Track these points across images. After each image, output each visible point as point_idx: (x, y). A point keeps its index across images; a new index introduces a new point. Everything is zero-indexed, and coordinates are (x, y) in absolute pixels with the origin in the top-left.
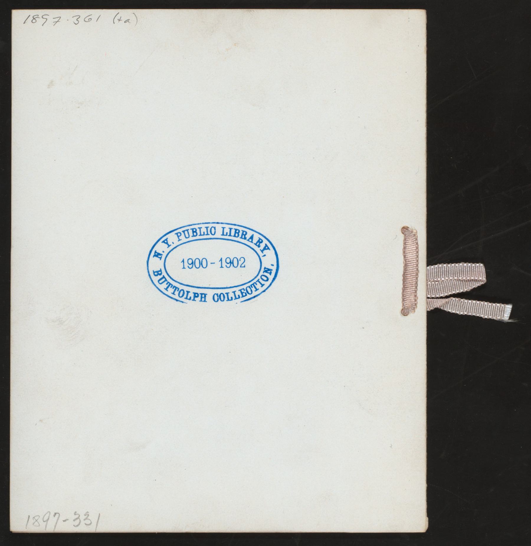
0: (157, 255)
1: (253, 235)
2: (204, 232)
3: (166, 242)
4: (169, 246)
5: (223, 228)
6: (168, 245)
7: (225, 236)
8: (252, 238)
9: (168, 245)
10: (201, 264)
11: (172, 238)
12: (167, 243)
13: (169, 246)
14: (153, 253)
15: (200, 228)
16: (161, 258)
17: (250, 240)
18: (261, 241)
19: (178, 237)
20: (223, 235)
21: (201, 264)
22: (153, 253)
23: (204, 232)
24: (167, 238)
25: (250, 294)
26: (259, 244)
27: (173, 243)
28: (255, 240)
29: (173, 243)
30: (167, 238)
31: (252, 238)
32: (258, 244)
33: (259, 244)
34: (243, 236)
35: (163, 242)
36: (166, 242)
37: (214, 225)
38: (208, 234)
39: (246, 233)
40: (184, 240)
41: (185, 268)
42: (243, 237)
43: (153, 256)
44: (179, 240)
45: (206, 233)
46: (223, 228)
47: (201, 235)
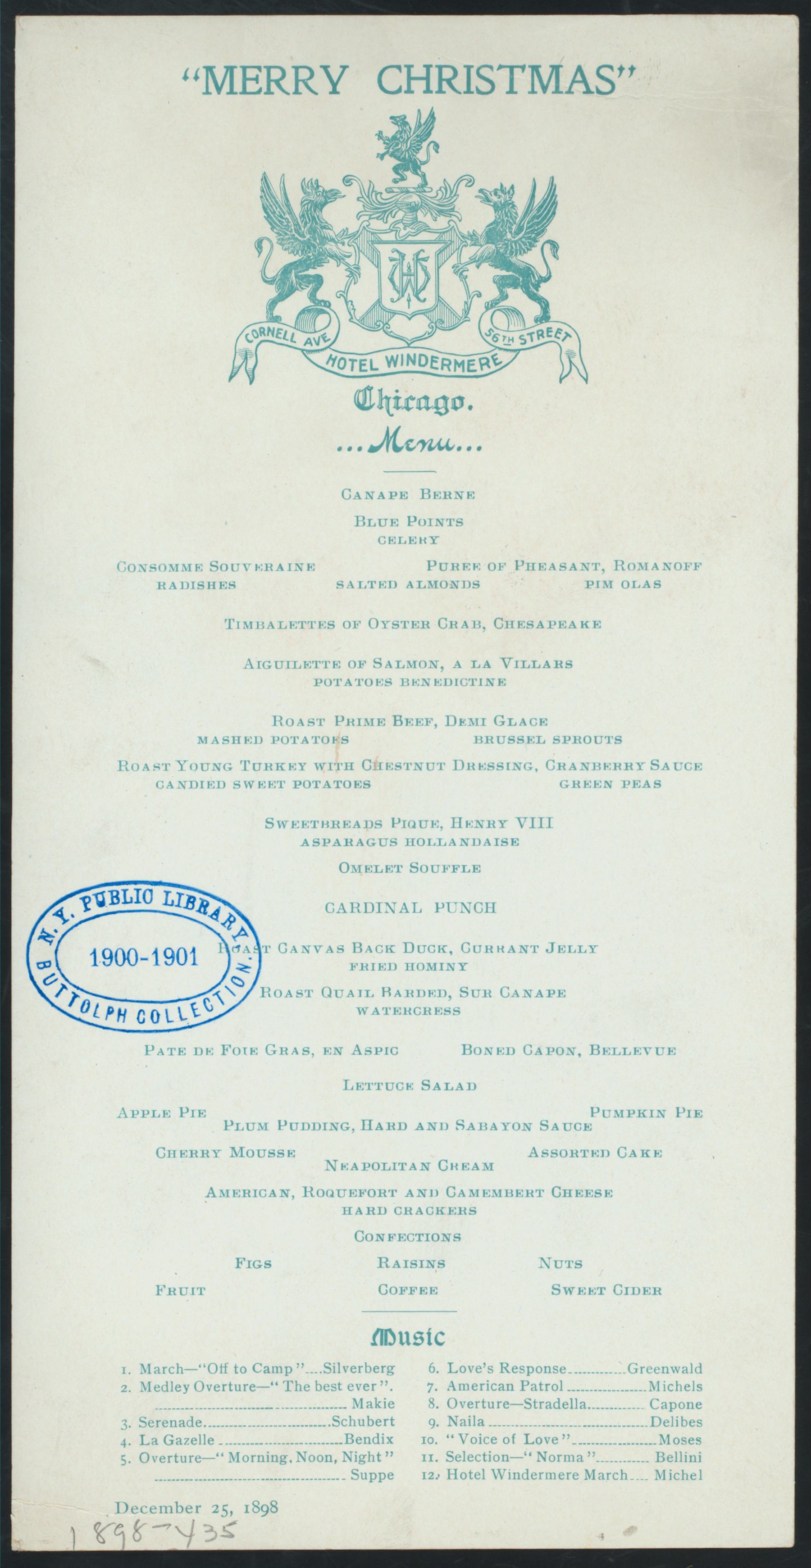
0: (45, 936)
1: (220, 907)
2: (131, 898)
3: (60, 914)
4: (65, 921)
5: (167, 893)
6: (63, 919)
7: (169, 910)
8: (217, 913)
9: (63, 919)
10: (126, 958)
11: (73, 907)
12: (61, 916)
13: (65, 921)
14: (38, 933)
15: (125, 891)
16: (51, 942)
17: (214, 917)
18: (205, 903)
19: (85, 905)
20: (166, 904)
21: (126, 958)
22: (38, 933)
23: (131, 898)
24: (62, 908)
25: (147, 903)
26: (205, 910)
27: (73, 916)
28: (223, 916)
29: (73, 916)
30: (62, 908)
31: (217, 913)
32: (202, 910)
33: (229, 926)
34: (228, 923)
35: (56, 914)
36: (60, 914)
37: (150, 887)
38: (138, 902)
39: (208, 905)
40: (95, 910)
41: (321, 67)
42: (202, 910)
43: (38, 936)
44: (87, 909)
45: (135, 900)
46: (167, 893)
47: (125, 902)
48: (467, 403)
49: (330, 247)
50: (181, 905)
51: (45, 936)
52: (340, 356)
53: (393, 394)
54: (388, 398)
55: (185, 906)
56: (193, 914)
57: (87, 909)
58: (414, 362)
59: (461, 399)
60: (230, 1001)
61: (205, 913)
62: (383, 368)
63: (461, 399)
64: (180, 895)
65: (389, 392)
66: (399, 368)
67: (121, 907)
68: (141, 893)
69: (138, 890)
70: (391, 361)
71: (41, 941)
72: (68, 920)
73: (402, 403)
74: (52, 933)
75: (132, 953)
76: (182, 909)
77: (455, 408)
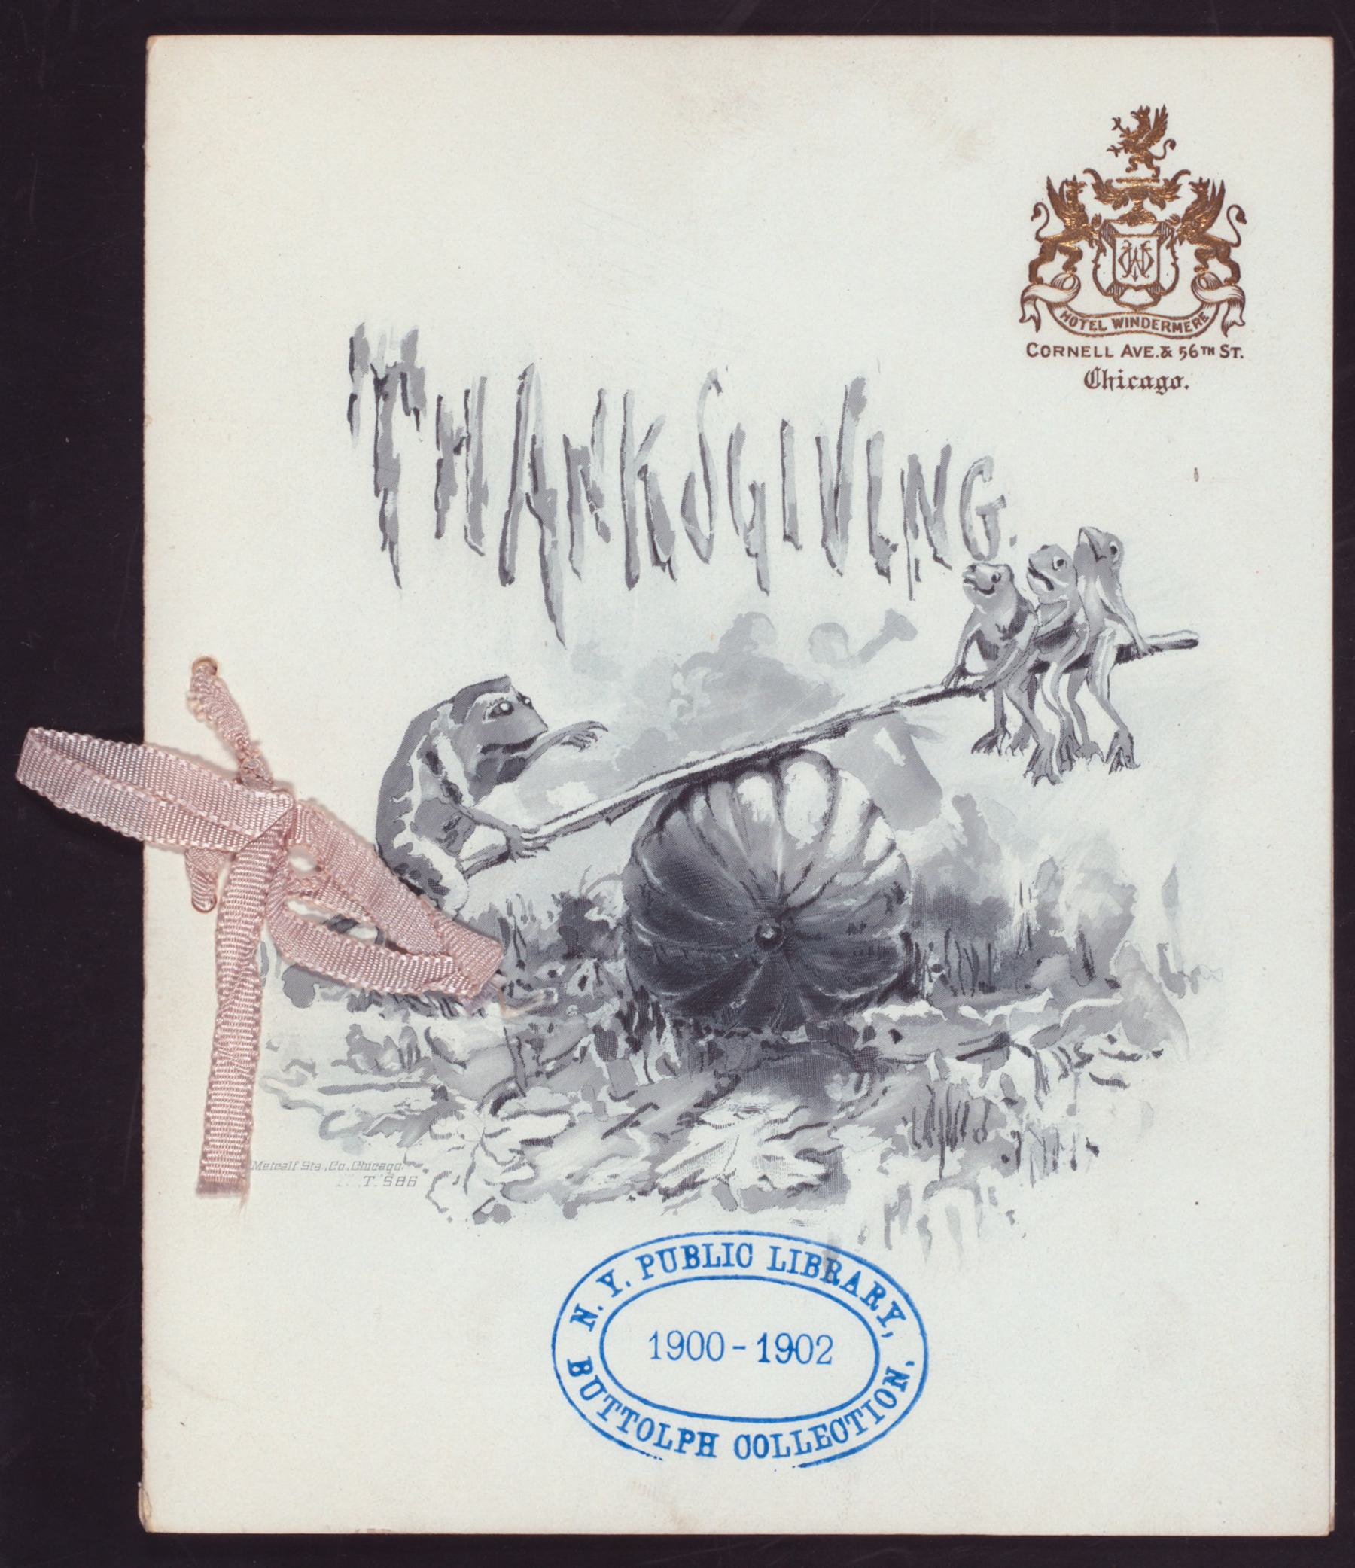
1: (859, 1273)
5: (775, 1249)
8: (854, 1281)
10: (705, 1345)
12: (611, 1284)
13: (617, 1292)
17: (850, 1288)
20: (773, 1268)
21: (705, 1345)
27: (628, 1284)
28: (865, 1287)
29: (628, 1284)
31: (854, 1281)
36: (607, 1280)
38: (728, 1264)
44: (647, 1276)
47: (708, 1264)
48: (1183, 383)
49: (867, 1078)
50: (797, 1269)
51: (583, 1316)
52: (1074, 315)
53: (1116, 374)
54: (1111, 379)
55: (803, 1270)
56: (816, 1283)
57: (647, 1276)
58: (1138, 325)
59: (1179, 379)
60: (874, 1430)
61: (836, 1282)
62: (1111, 329)
63: (1179, 379)
64: (795, 1252)
65: (1113, 373)
66: (1124, 328)
67: (700, 1271)
68: (733, 1250)
69: (728, 1246)
70: (1117, 324)
72: (620, 1291)
73: (1126, 383)
74: (594, 1310)
75: (715, 1339)
76: (799, 1276)
77: (1173, 387)
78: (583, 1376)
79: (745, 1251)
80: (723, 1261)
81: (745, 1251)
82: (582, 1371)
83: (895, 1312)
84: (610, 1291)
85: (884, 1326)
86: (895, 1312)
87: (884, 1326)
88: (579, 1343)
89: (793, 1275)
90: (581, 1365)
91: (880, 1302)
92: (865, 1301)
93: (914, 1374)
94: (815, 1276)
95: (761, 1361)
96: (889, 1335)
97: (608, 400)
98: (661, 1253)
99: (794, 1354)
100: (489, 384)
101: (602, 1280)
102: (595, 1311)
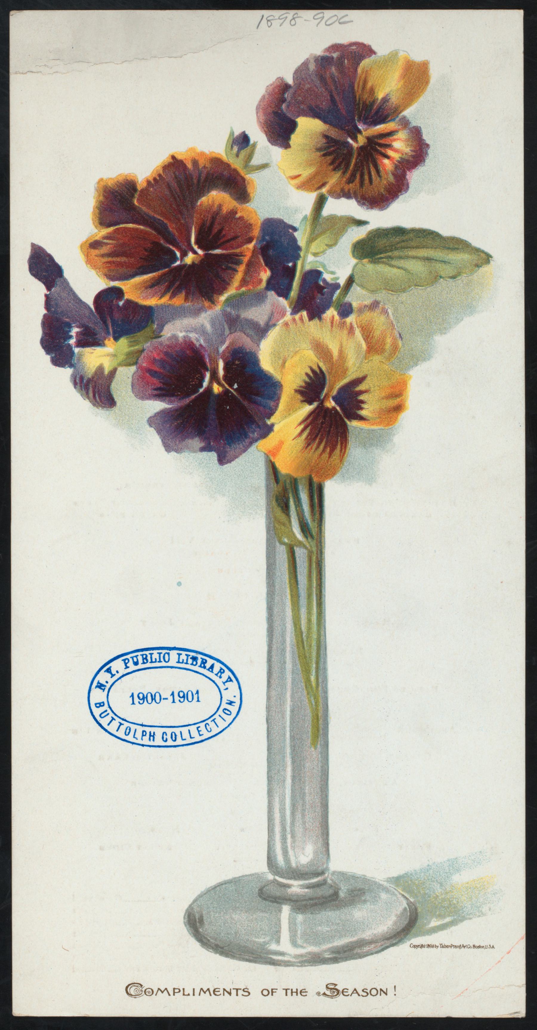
8: (212, 667)
20: (178, 662)
31: (212, 667)
38: (160, 661)
44: (127, 667)
47: (152, 662)
50: (188, 662)
51: (100, 686)
61: (205, 667)
68: (162, 655)
69: (160, 654)
71: (98, 689)
78: (101, 708)
79: (167, 656)
80: (158, 660)
81: (167, 656)
82: (101, 706)
83: (229, 680)
84: (110, 675)
85: (225, 685)
86: (229, 680)
87: (225, 685)
88: (98, 696)
89: (187, 665)
90: (100, 704)
91: (223, 675)
92: (216, 675)
93: (237, 700)
94: (196, 665)
95: (132, 704)
96: (227, 689)
97: (291, 994)
98: (132, 658)
99: (145, 700)
100: (351, 23)
101: (229, 678)
102: (105, 684)
